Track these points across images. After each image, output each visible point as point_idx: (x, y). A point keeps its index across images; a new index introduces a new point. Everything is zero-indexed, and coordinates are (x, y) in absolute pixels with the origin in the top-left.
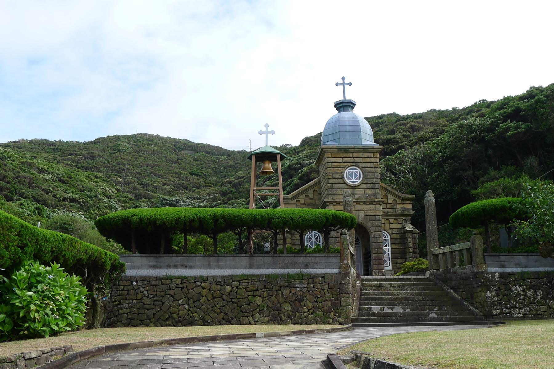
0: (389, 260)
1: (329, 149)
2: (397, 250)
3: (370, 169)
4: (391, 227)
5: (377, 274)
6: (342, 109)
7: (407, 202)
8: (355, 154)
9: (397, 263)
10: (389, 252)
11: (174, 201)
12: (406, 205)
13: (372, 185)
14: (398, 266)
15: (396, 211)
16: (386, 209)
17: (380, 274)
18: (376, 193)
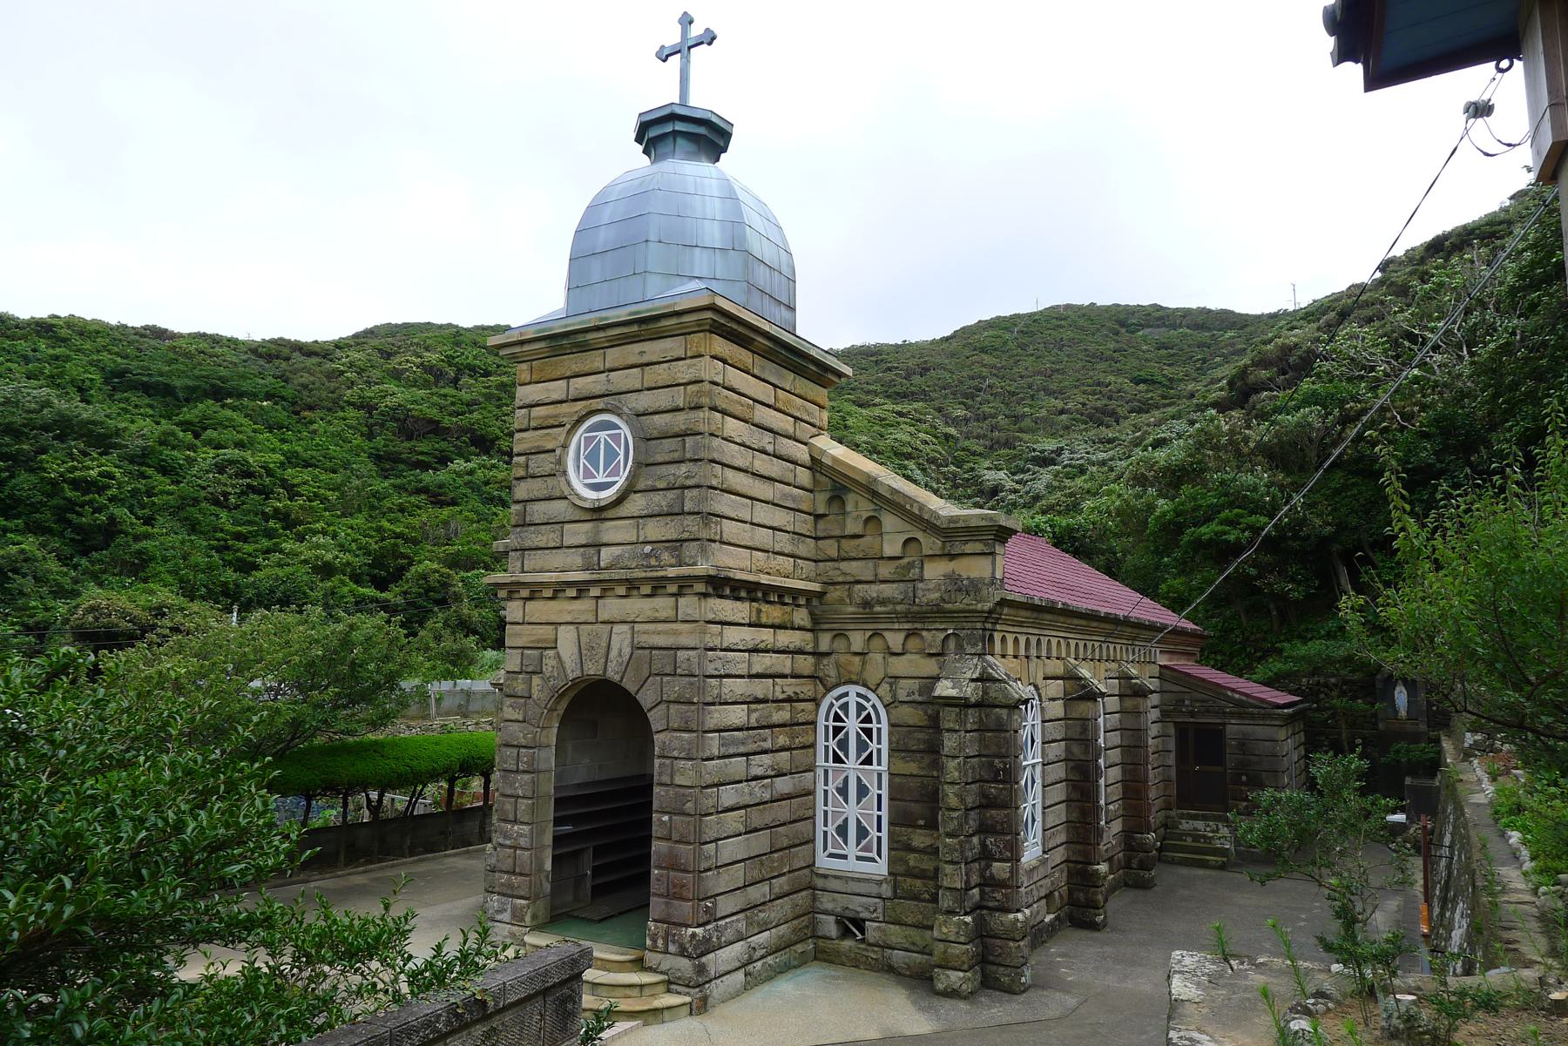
0: (879, 830)
1: (517, 349)
2: (913, 783)
3: (667, 417)
4: (893, 671)
5: (660, 942)
6: (667, 146)
7: (969, 548)
8: (614, 356)
9: (909, 849)
10: (880, 788)
11: (1052, 452)
12: (965, 561)
13: (671, 495)
14: (912, 863)
15: (920, 593)
16: (874, 587)
17: (672, 948)
18: (685, 536)
